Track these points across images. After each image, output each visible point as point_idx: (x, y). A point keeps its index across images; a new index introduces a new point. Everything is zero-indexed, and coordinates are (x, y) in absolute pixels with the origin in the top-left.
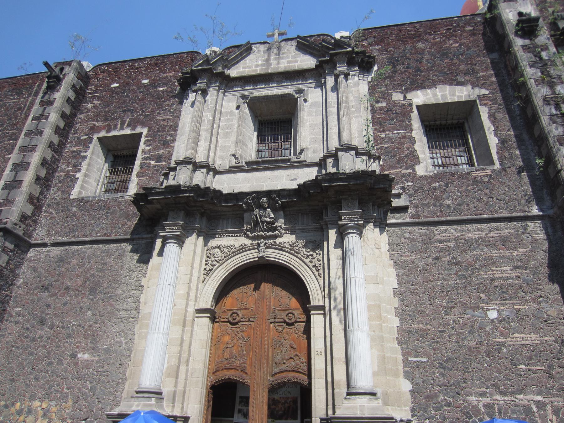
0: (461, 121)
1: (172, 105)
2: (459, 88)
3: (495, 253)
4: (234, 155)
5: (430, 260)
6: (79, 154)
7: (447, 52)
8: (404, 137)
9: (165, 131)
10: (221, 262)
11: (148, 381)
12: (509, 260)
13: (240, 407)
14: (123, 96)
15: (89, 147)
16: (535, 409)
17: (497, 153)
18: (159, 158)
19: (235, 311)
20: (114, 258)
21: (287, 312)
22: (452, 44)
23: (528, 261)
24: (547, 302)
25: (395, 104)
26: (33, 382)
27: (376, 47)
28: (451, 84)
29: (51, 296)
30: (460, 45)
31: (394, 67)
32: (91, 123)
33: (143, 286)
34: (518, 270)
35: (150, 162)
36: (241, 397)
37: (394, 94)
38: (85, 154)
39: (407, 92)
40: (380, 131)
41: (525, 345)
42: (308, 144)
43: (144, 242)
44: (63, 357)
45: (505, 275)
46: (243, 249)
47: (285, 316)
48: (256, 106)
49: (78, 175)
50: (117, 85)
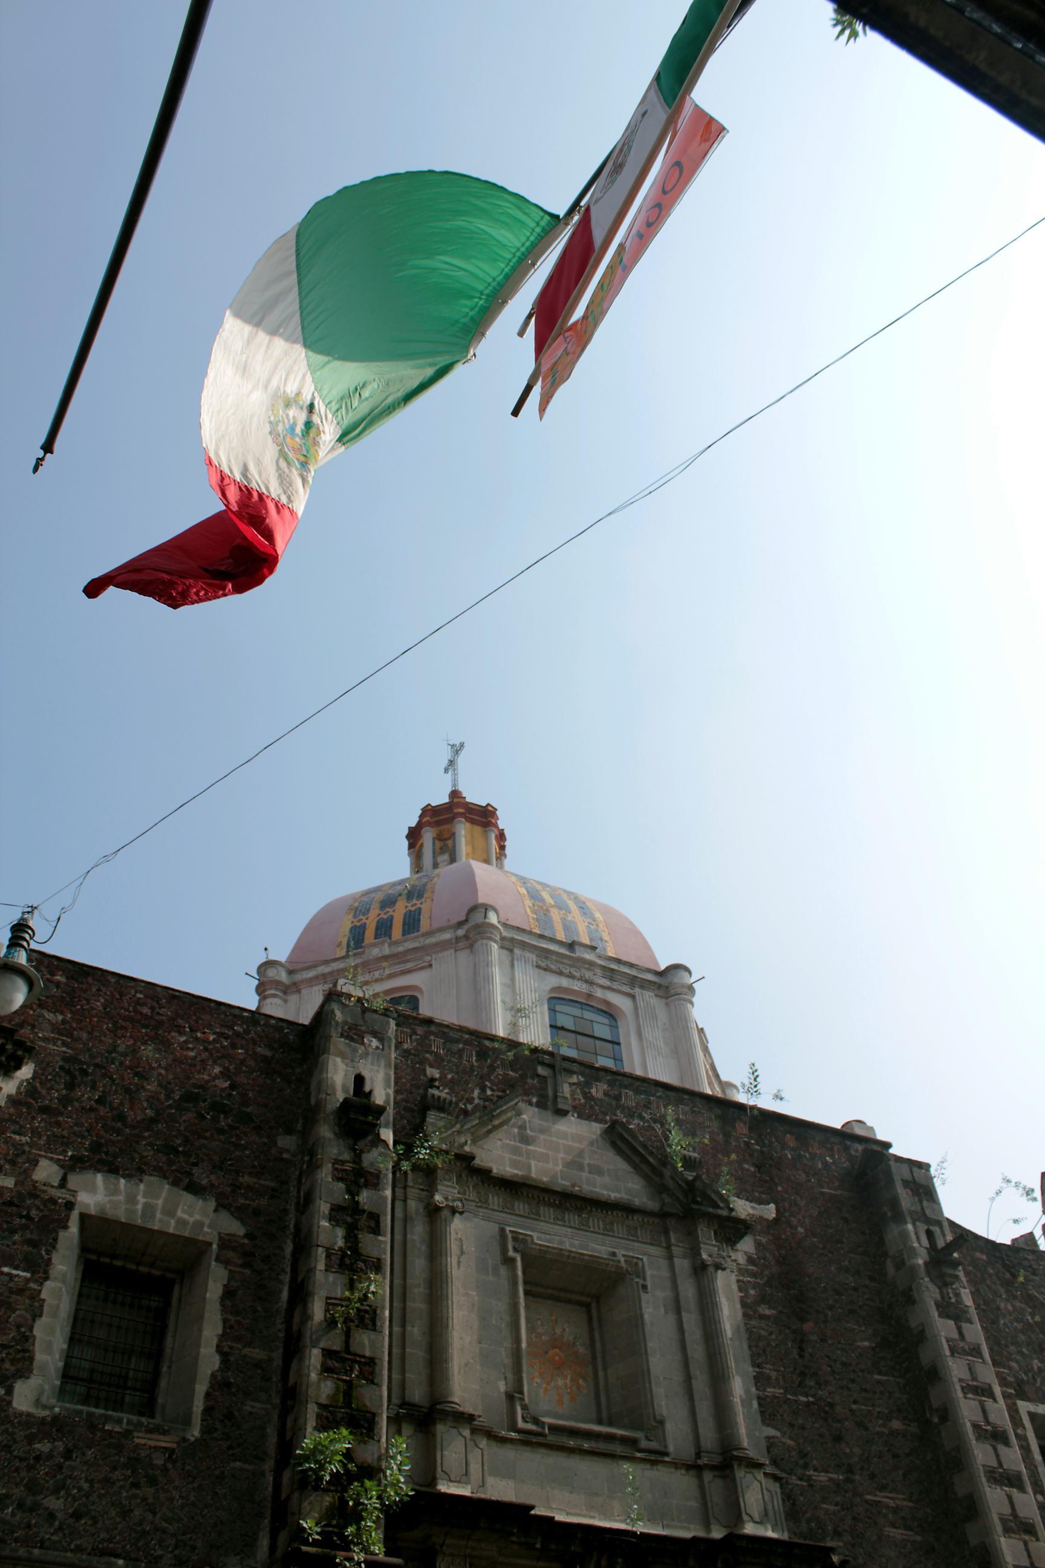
2: (188, 1198)
8: (20, 1291)
17: (208, 1395)
28: (175, 1183)
30: (232, 1087)
31: (71, 1086)
37: (44, 1163)
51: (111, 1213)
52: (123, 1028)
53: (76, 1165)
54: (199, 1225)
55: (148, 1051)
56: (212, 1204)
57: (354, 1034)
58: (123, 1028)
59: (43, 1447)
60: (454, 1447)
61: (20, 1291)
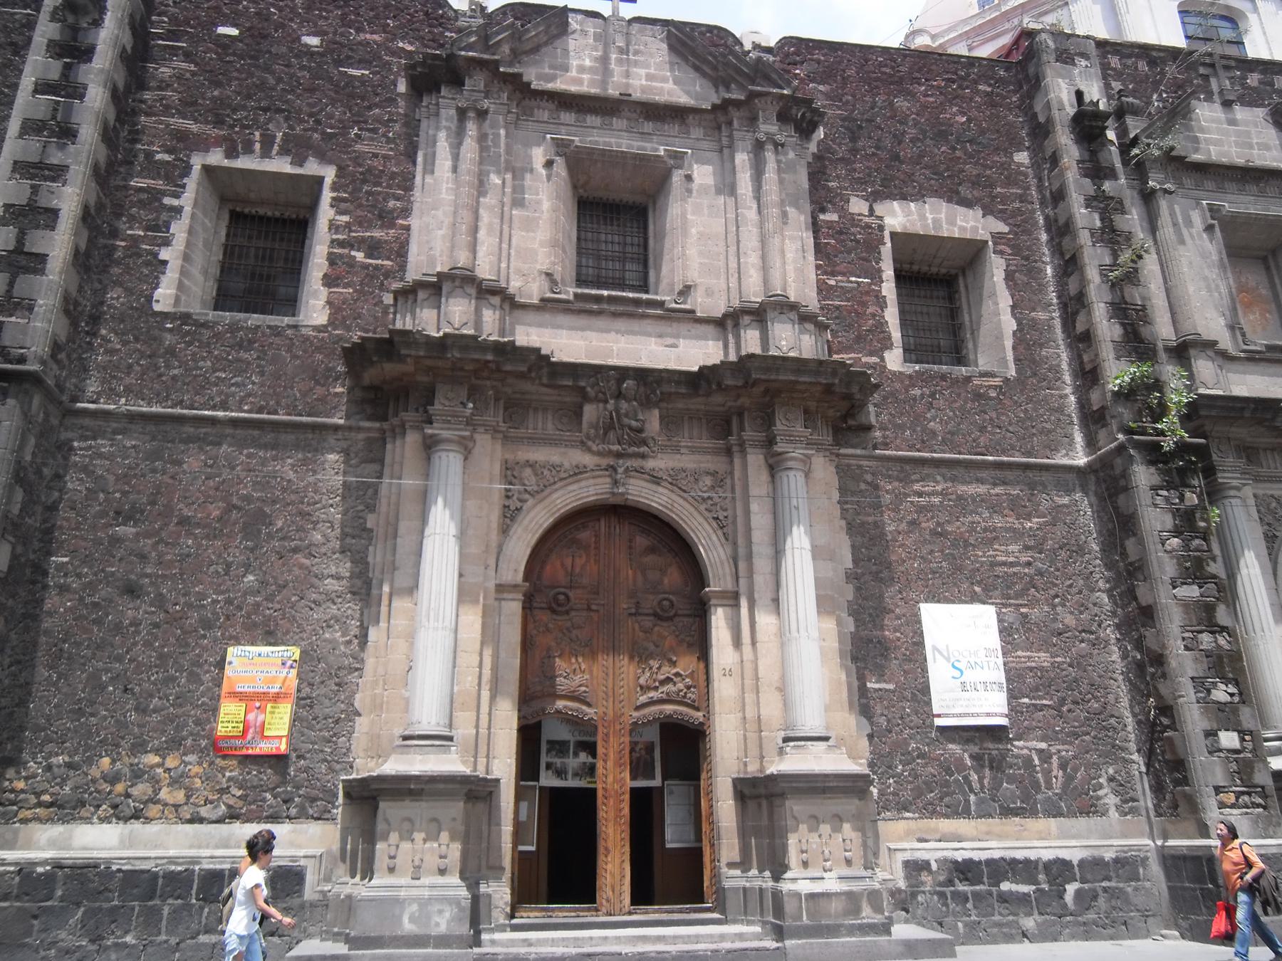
0: (953, 272)
1: (390, 120)
2: (961, 210)
3: (998, 521)
4: (548, 274)
5: (903, 526)
6: (160, 200)
7: (945, 131)
8: (867, 293)
9: (380, 184)
10: (539, 493)
11: (428, 717)
12: (1017, 535)
13: (550, 760)
14: (257, 67)
15: (184, 186)
16: (1037, 762)
17: (1014, 348)
18: (373, 248)
19: (562, 590)
20: (293, 466)
21: (662, 596)
22: (955, 115)
23: (1045, 539)
24: (1064, 606)
25: (853, 220)
26: (133, 716)
27: (821, 88)
28: (949, 201)
29: (147, 535)
30: (969, 120)
31: (854, 139)
32: (177, 122)
33: (371, 530)
34: (1030, 553)
35: (353, 253)
36: (549, 742)
37: (853, 200)
38: (175, 202)
39: (875, 201)
40: (825, 273)
41: (1031, 669)
42: (696, 274)
43: (361, 436)
44: (200, 666)
45: (1011, 559)
46: (578, 472)
47: (655, 603)
48: (578, 163)
49: (164, 254)
50: (234, 32)
51: (911, 230)
52: (877, 87)
53: (874, 197)
54: (975, 229)
55: (901, 103)
56: (980, 212)
57: (1066, 57)
58: (877, 87)
59: (916, 392)
60: (1204, 367)
61: (867, 293)
